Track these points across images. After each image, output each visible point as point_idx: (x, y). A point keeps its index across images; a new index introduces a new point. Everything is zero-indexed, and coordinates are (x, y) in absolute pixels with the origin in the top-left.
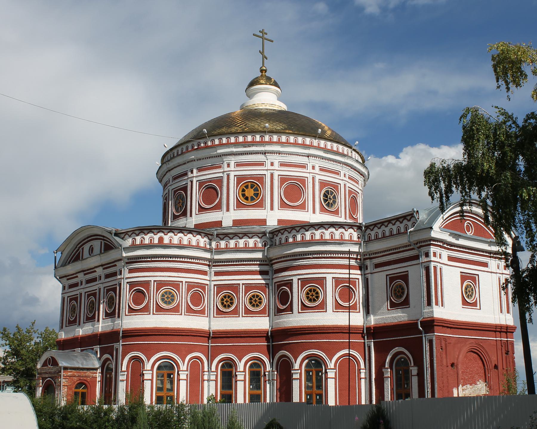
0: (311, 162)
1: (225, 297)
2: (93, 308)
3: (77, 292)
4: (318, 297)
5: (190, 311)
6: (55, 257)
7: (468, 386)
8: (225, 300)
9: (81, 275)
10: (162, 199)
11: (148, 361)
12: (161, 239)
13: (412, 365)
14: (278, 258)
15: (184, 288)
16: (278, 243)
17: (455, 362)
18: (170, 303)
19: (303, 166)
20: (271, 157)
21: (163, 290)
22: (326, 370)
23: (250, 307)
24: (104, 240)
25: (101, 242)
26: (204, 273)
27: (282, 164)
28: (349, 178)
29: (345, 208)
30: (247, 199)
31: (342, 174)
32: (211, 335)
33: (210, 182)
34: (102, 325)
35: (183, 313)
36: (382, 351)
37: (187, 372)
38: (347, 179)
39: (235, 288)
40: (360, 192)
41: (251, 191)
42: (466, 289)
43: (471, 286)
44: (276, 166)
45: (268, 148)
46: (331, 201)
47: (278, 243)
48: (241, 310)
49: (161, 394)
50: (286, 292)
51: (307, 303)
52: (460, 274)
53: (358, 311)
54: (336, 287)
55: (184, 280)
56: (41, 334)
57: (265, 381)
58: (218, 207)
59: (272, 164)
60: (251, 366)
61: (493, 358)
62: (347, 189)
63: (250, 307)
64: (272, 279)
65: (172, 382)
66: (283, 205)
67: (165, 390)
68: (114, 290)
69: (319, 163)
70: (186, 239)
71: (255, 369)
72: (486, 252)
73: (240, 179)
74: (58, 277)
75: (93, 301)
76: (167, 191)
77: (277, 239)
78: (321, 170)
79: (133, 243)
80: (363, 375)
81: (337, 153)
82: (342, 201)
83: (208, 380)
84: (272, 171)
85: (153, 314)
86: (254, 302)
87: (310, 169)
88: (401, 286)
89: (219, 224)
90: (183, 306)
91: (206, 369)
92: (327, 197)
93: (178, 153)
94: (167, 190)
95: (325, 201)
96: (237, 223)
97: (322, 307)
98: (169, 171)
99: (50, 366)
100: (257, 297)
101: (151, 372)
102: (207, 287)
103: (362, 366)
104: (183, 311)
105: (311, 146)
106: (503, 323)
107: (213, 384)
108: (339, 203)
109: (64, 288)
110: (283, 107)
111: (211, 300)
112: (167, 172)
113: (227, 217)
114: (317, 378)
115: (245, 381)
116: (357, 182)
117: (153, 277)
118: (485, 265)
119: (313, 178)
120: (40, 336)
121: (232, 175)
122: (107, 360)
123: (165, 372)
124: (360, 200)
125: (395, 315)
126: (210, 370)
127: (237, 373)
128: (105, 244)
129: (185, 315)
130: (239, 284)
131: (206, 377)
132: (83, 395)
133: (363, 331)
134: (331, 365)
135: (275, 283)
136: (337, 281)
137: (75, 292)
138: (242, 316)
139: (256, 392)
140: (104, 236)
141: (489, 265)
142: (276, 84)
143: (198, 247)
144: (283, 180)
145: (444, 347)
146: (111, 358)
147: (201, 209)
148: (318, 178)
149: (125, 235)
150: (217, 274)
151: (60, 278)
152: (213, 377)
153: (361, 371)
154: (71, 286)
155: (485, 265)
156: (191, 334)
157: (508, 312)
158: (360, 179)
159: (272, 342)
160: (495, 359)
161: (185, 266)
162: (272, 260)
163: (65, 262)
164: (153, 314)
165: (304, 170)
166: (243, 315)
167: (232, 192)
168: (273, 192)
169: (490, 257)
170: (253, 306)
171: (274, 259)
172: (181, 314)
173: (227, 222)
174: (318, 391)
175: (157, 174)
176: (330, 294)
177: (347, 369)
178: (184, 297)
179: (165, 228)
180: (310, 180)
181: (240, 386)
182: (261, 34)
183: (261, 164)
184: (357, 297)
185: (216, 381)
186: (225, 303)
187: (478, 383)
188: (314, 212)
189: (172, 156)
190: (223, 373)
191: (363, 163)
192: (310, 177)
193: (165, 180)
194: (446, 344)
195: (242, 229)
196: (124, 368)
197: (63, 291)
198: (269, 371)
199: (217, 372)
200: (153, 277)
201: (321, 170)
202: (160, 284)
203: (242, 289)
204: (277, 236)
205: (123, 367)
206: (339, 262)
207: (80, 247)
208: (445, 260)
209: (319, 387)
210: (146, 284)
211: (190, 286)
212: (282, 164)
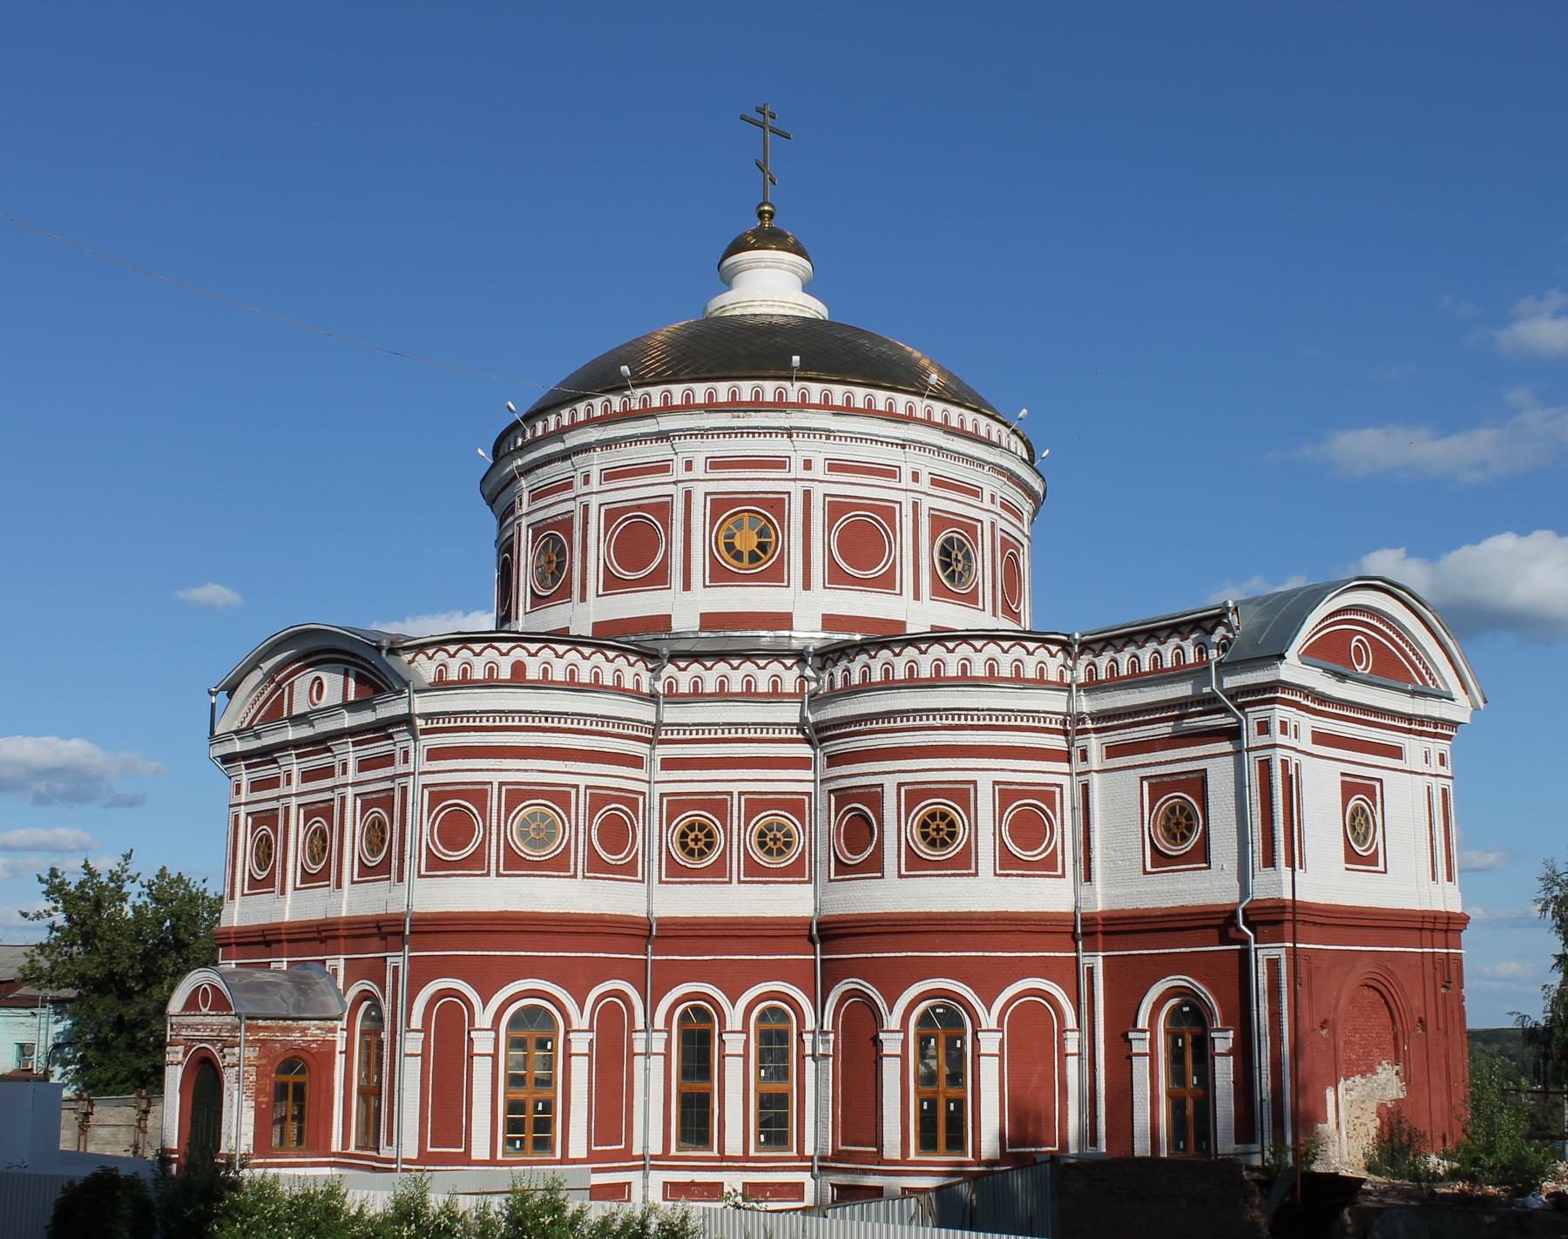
0: (907, 461)
1: (691, 827)
4: (952, 835)
5: (597, 866)
6: (213, 705)
7: (1358, 1078)
8: (692, 836)
10: (494, 551)
12: (519, 668)
13: (1218, 1024)
15: (581, 803)
17: (1330, 1017)
18: (544, 844)
20: (687, 447)
21: (524, 810)
22: (975, 1033)
23: (759, 857)
26: (635, 761)
27: (834, 467)
28: (1003, 506)
29: (994, 586)
30: (738, 556)
31: (987, 497)
34: (351, 900)
35: (580, 873)
36: (1126, 987)
37: (590, 1036)
38: (998, 509)
39: (718, 805)
40: (1025, 541)
41: (751, 540)
42: (1353, 818)
43: (1363, 810)
44: (819, 470)
45: (667, 423)
46: (960, 568)
48: (736, 864)
49: (519, 1094)
51: (923, 850)
52: (1340, 778)
53: (1060, 872)
54: (1003, 810)
56: (149, 887)
58: (659, 578)
60: (762, 1017)
61: (1414, 1000)
62: (999, 534)
63: (759, 857)
65: (549, 1063)
66: (837, 577)
67: (530, 1082)
69: (930, 465)
70: (560, 663)
71: (773, 1025)
72: (1410, 718)
73: (719, 505)
78: (935, 482)
79: (441, 676)
80: (1071, 1047)
81: (974, 438)
82: (985, 568)
83: (647, 1054)
85: (499, 875)
86: (771, 844)
88: (1184, 808)
89: (664, 622)
91: (639, 1024)
92: (949, 555)
95: (946, 566)
96: (710, 621)
97: (964, 863)
99: (205, 1010)
101: (492, 1034)
102: (641, 799)
103: (1071, 1022)
104: (580, 867)
105: (908, 419)
106: (1439, 906)
107: (657, 1064)
108: (980, 574)
110: (815, 308)
111: (654, 837)
113: (685, 606)
114: (948, 1055)
115: (746, 1056)
116: (1018, 515)
117: (496, 774)
118: (1396, 752)
119: (915, 505)
120: (146, 890)
121: (699, 491)
123: (530, 1034)
124: (1025, 563)
125: (1166, 888)
130: (730, 794)
131: (639, 1047)
132: (299, 1091)
133: (1075, 927)
134: (989, 1020)
136: (1007, 795)
138: (740, 882)
139: (776, 1087)
140: (354, 655)
141: (1406, 753)
142: (799, 251)
144: (836, 508)
145: (1441, 1026)
146: (375, 990)
147: (612, 584)
148: (818, 492)
150: (668, 764)
152: (658, 1046)
155: (1396, 752)
157: (1450, 879)
158: (1027, 507)
160: (1419, 1003)
164: (499, 875)
168: (809, 541)
169: (1410, 731)
170: (769, 852)
171: (828, 728)
172: (575, 876)
173: (685, 620)
174: (953, 1092)
175: (483, 480)
176: (986, 828)
177: (1031, 1034)
179: (505, 633)
180: (908, 510)
181: (734, 1068)
183: (779, 464)
184: (1057, 836)
186: (692, 844)
187: (1380, 1069)
190: (687, 1037)
191: (1030, 462)
192: (907, 500)
194: (1309, 972)
195: (726, 640)
196: (416, 1022)
198: (814, 1032)
199: (669, 1033)
200: (496, 774)
201: (937, 482)
203: (737, 809)
208: (1305, 742)
209: (956, 1078)
210: (478, 795)
211: (598, 799)
212: (834, 467)
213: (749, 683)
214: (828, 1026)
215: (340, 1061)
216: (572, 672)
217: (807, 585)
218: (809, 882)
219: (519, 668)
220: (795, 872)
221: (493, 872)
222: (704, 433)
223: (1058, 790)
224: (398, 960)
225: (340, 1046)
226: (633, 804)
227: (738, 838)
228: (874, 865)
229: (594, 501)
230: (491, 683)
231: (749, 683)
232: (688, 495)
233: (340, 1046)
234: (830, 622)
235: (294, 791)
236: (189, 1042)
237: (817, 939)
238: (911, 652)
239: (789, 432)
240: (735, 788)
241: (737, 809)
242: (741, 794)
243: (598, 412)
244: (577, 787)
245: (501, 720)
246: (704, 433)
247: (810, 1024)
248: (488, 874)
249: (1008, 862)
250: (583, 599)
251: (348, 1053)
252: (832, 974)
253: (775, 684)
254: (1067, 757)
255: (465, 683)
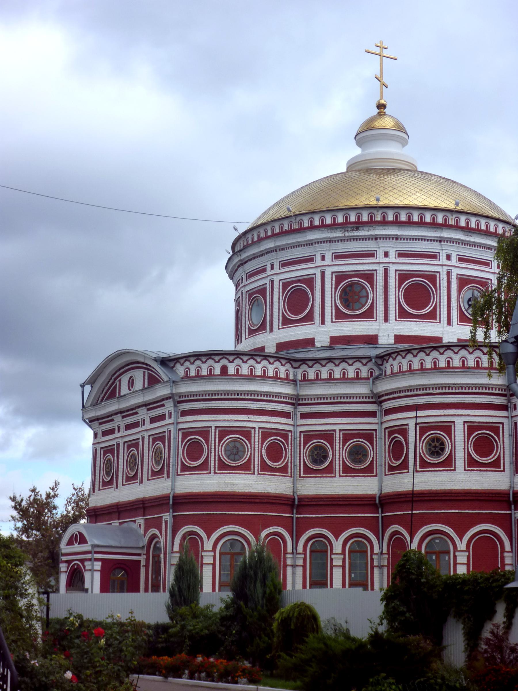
0: (444, 250)
2: (161, 458)
3: (114, 442)
4: (443, 450)
5: (265, 468)
9: (118, 419)
11: (209, 538)
12: (224, 369)
14: (392, 393)
15: (257, 436)
16: (388, 372)
19: (433, 256)
24: (148, 369)
25: (144, 372)
27: (401, 255)
32: (296, 502)
33: (299, 281)
35: (256, 472)
39: (329, 436)
44: (392, 257)
47: (388, 372)
50: (400, 442)
53: (502, 469)
54: (469, 435)
55: (257, 426)
57: (372, 567)
58: (309, 318)
59: (386, 255)
64: (382, 423)
66: (403, 314)
68: (136, 445)
69: (455, 251)
74: (87, 421)
75: (134, 455)
76: (239, 294)
77: (388, 366)
83: (294, 566)
84: (386, 265)
87: (443, 260)
89: (310, 342)
90: (256, 462)
91: (290, 549)
93: (253, 239)
94: (240, 293)
96: (336, 341)
97: (448, 463)
98: (242, 264)
100: (433, 441)
103: (508, 547)
104: (256, 469)
107: (299, 571)
109: (96, 436)
111: (297, 454)
112: (239, 267)
115: (344, 567)
119: (449, 274)
122: (154, 537)
126: (295, 551)
127: (333, 556)
128: (150, 375)
129: (258, 474)
130: (335, 431)
131: (289, 562)
135: (386, 429)
137: (109, 440)
138: (340, 476)
140: (147, 365)
143: (276, 378)
144: (403, 277)
147: (286, 322)
148: (455, 272)
149: (176, 363)
151: (91, 422)
152: (300, 562)
153: (506, 554)
154: (105, 433)
156: (268, 501)
159: (382, 513)
161: (258, 406)
162: (380, 397)
163: (97, 399)
165: (434, 262)
166: (341, 474)
167: (327, 297)
171: (383, 396)
172: (254, 473)
176: (460, 445)
178: (256, 449)
180: (444, 277)
182: (377, 50)
183: (371, 255)
185: (304, 567)
188: (449, 323)
189: (245, 244)
193: (237, 276)
197: (94, 440)
199: (305, 554)
201: (461, 259)
202: (224, 432)
203: (338, 438)
204: (387, 362)
205: (175, 546)
206: (474, 399)
207: (115, 379)
210: (205, 433)
211: (266, 434)
212: (401, 255)
213: (344, 373)
214: (385, 551)
215: (143, 571)
216: (251, 370)
217: (386, 320)
218: (376, 476)
219: (224, 369)
220: (369, 470)
221: (212, 472)
222: (330, 241)
223: (501, 426)
224: (167, 517)
225: (143, 563)
226: (285, 437)
227: (339, 453)
228: (404, 466)
229: (276, 279)
230: (211, 376)
231: (344, 373)
232: (323, 273)
233: (143, 563)
234: (399, 339)
235: (145, 432)
236: (68, 562)
237: (379, 505)
238: (449, 353)
239: (376, 238)
240: (337, 428)
241: (338, 438)
242: (340, 430)
243: (277, 231)
244: (254, 428)
245: (215, 396)
246: (330, 241)
247: (376, 550)
248: (210, 473)
249: (472, 463)
250: (272, 330)
251: (147, 566)
252: (387, 522)
253: (357, 373)
254: (504, 408)
255: (198, 377)
